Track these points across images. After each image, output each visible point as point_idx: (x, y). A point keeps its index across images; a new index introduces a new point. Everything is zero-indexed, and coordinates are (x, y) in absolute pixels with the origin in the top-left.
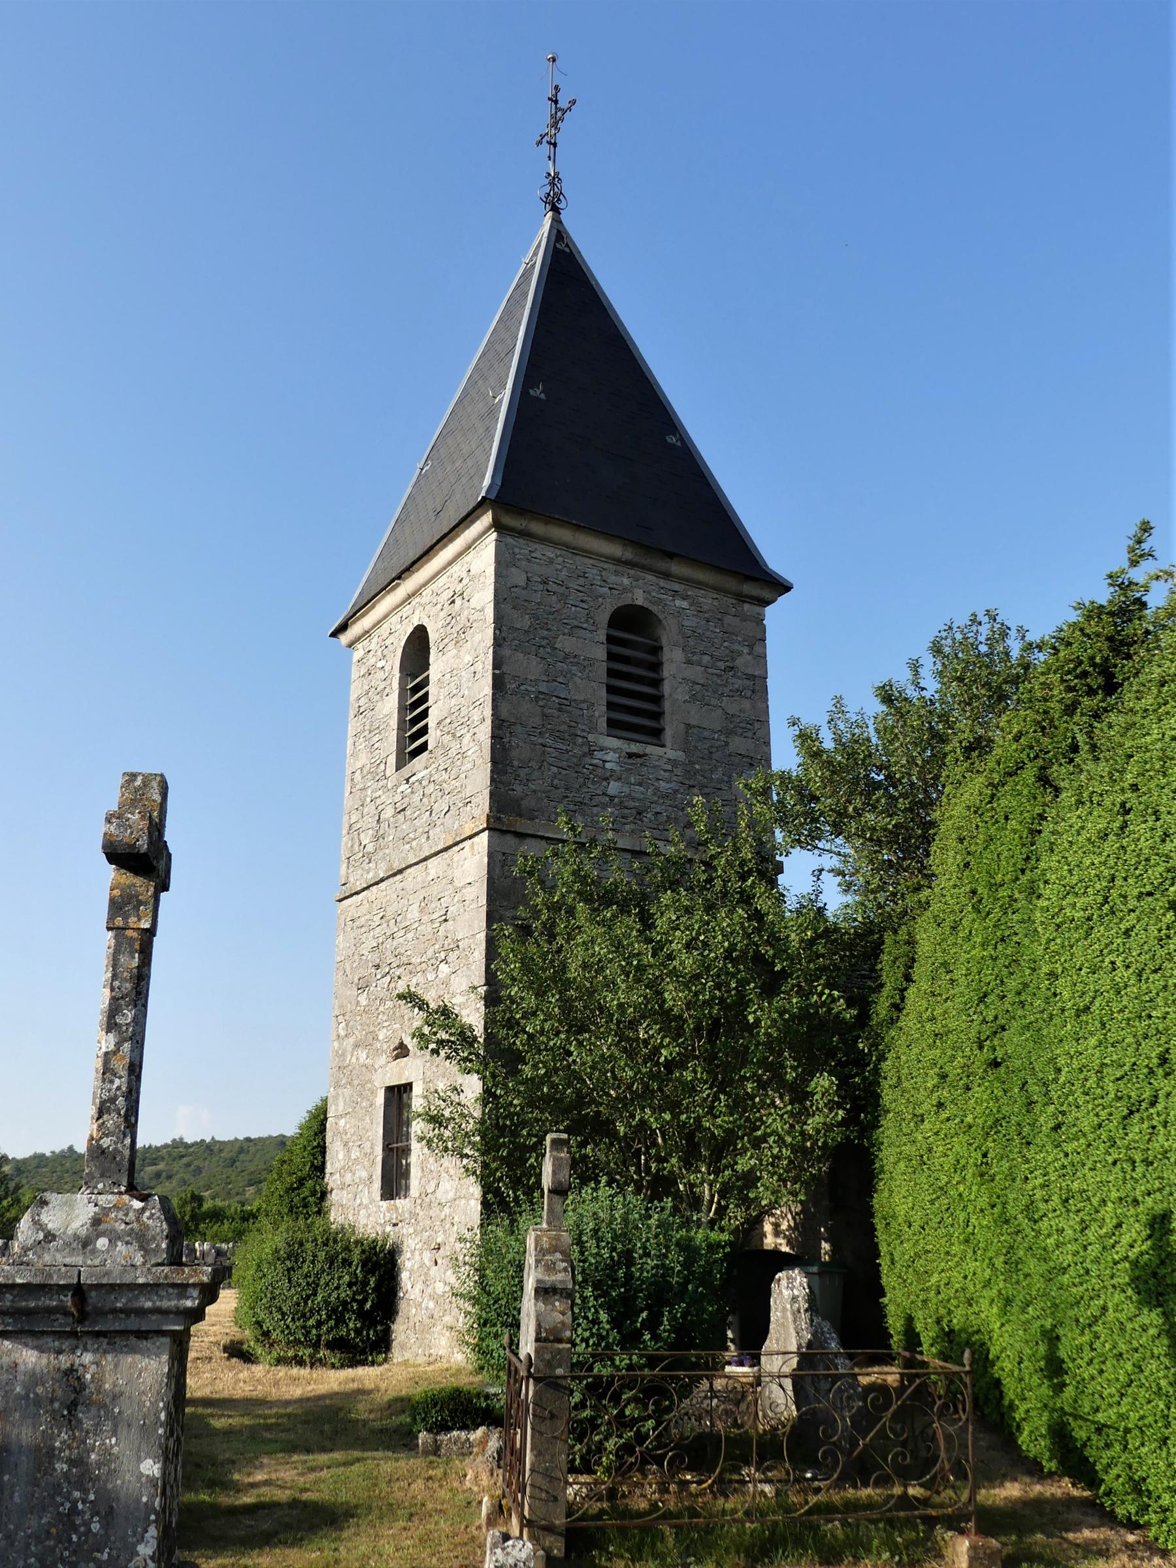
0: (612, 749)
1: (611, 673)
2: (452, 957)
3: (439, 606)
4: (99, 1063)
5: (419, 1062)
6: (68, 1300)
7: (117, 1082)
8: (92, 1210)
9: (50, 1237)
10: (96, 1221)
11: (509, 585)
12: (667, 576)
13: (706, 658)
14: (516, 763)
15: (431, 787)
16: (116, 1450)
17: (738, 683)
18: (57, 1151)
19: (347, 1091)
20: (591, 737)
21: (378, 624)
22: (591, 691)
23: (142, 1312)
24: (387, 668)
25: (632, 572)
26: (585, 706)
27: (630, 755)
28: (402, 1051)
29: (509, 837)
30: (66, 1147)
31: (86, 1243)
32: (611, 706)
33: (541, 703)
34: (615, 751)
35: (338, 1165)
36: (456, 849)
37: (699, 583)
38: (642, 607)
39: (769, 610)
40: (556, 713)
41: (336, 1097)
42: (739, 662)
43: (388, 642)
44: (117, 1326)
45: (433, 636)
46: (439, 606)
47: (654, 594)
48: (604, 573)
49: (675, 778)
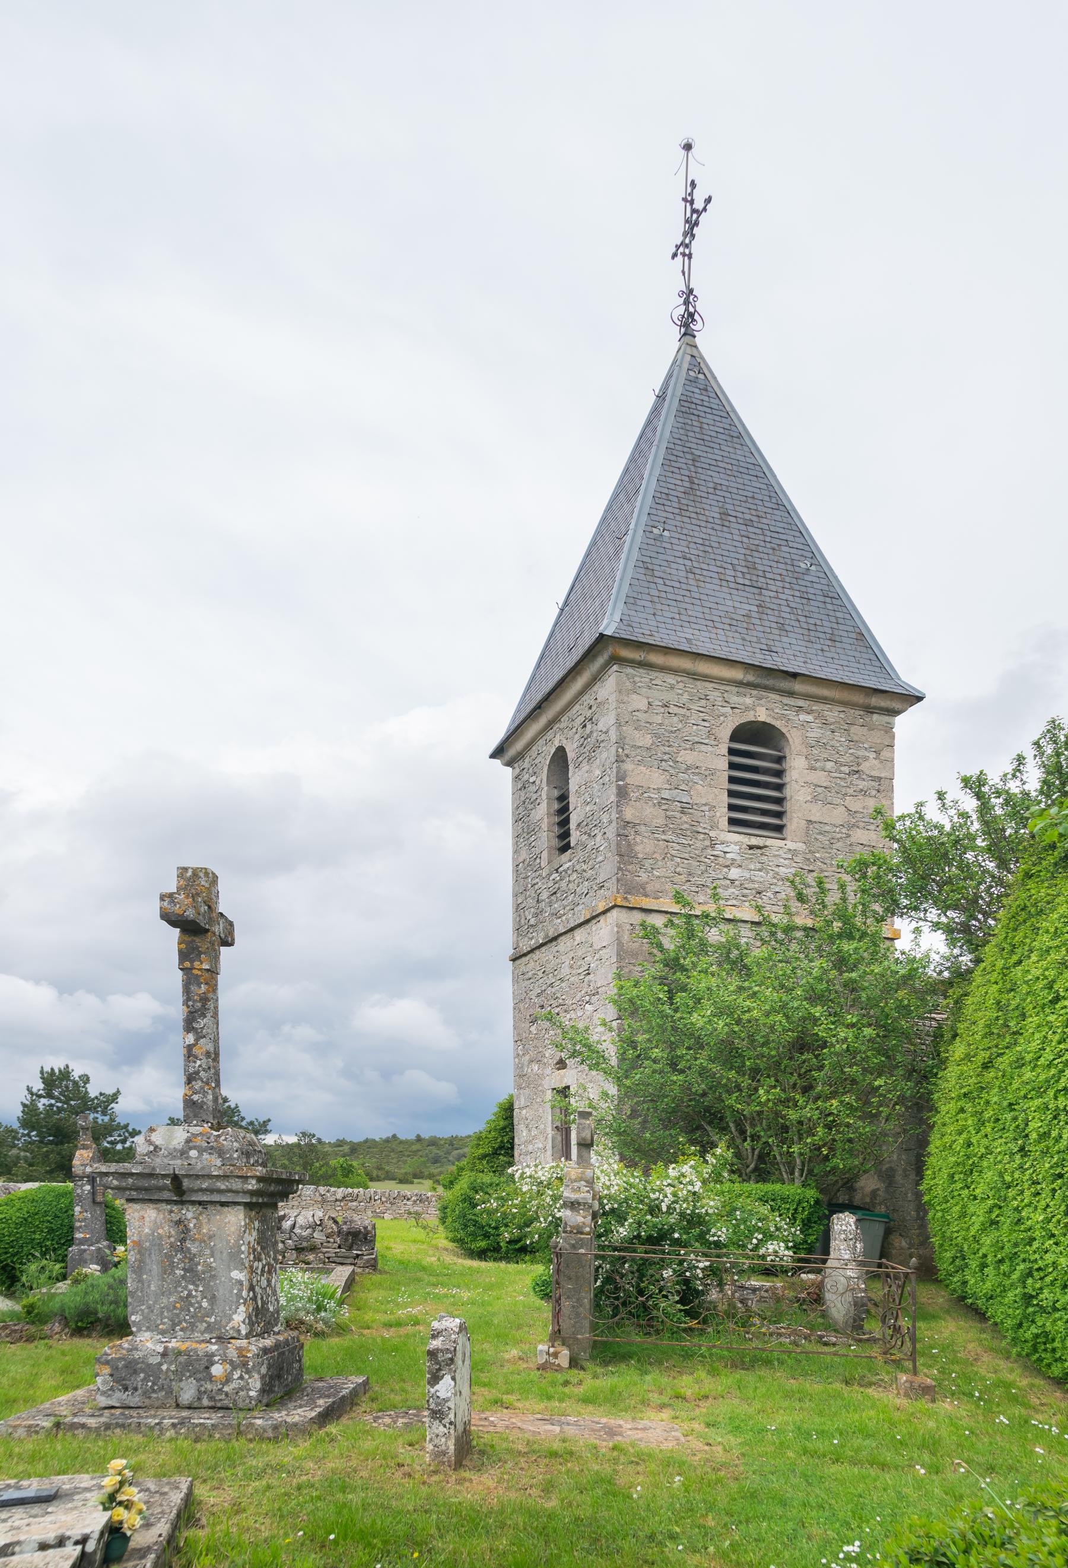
0: (734, 842)
1: (732, 780)
2: (594, 999)
3: (574, 730)
4: (183, 1051)
5: (574, 1072)
6: (168, 1182)
7: (198, 1063)
8: (186, 1135)
9: (157, 1148)
10: (188, 1141)
11: (630, 710)
12: (791, 694)
13: (829, 765)
14: (640, 856)
15: (575, 875)
16: (214, 1265)
17: (862, 785)
18: (384, 1137)
19: (527, 1091)
20: (712, 834)
21: (529, 746)
22: (715, 797)
23: (220, 1191)
24: (538, 783)
25: (754, 692)
26: (706, 808)
27: (751, 847)
28: (561, 1064)
29: (635, 912)
30: (390, 1135)
31: (183, 1153)
32: (732, 808)
33: (664, 807)
34: (736, 844)
35: (523, 1139)
36: (594, 921)
37: (825, 698)
38: (764, 723)
39: (899, 720)
40: (678, 815)
41: (518, 1097)
42: (865, 767)
43: (536, 761)
44: (205, 1198)
45: (571, 755)
46: (574, 730)
47: (777, 711)
48: (726, 695)
49: (795, 865)
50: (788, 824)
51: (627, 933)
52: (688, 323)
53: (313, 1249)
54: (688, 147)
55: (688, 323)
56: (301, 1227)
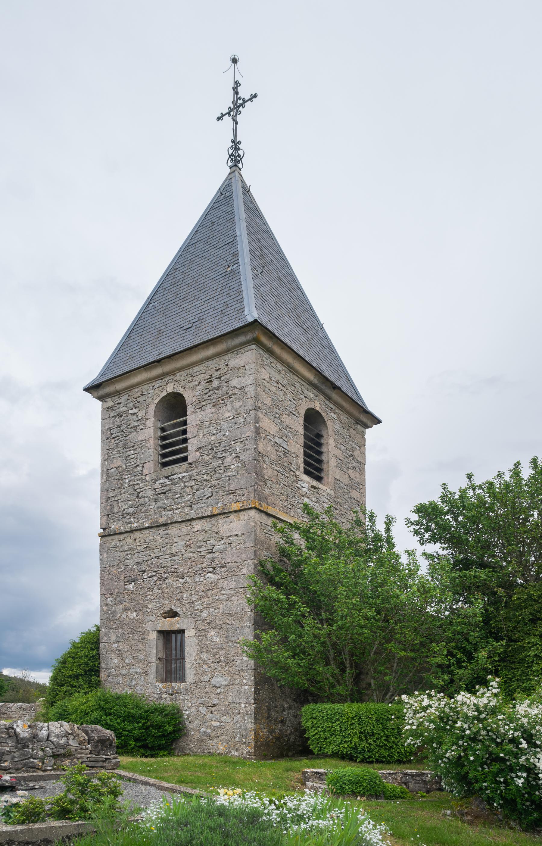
12: (329, 398)
38: (318, 412)
39: (368, 431)
50: (326, 478)
51: (259, 528)
52: (235, 159)
53: (68, 755)
54: (235, 61)
55: (235, 159)
56: (57, 736)
